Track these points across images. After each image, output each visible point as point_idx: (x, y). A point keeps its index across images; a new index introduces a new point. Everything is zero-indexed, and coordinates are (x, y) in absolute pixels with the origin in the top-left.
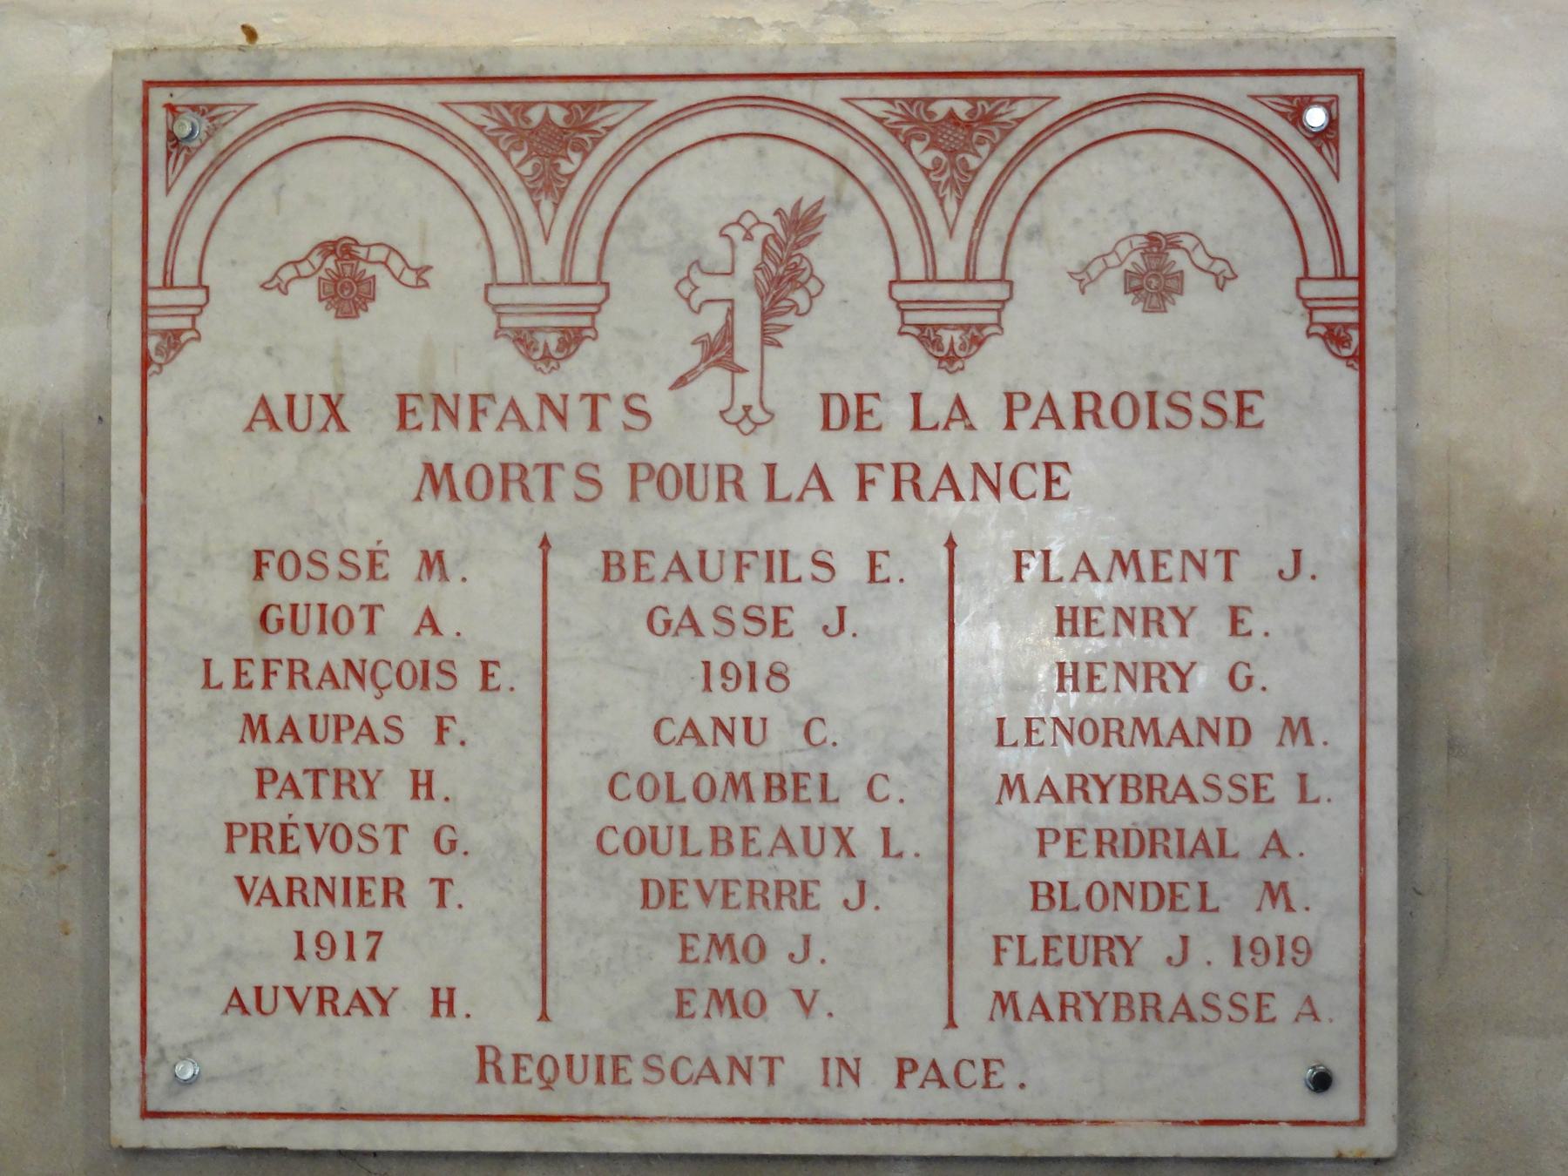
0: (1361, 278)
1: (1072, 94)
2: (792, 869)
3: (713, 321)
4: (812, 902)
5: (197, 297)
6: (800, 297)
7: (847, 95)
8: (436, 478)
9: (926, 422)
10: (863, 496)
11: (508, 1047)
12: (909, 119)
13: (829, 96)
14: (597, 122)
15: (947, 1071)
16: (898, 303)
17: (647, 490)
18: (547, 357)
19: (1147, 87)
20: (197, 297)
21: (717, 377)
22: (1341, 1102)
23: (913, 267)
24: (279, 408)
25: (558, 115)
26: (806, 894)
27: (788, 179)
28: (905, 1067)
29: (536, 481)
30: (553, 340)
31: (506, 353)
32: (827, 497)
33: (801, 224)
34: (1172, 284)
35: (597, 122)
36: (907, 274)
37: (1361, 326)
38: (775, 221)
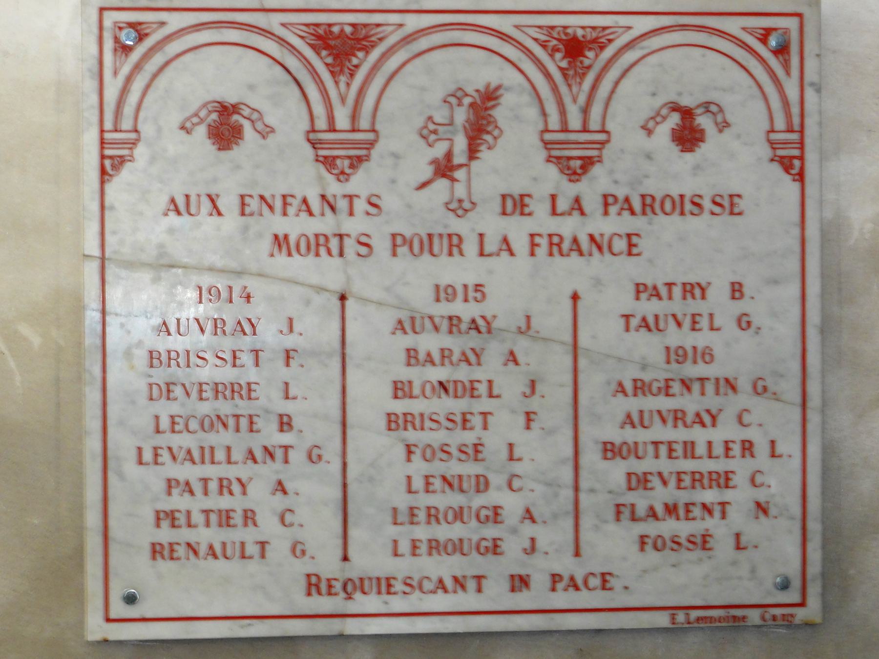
0: (802, 132)
1: (176, 21)
2: (719, 466)
3: (440, 150)
4: (731, 484)
5: (370, 136)
6: (488, 137)
7: (517, 24)
8: (280, 242)
9: (559, 210)
10: (532, 254)
11: (325, 575)
12: (366, 38)
13: (732, 26)
14: (373, 35)
15: (580, 582)
16: (772, 143)
17: (403, 250)
18: (575, 173)
19: (459, 23)
20: (370, 136)
21: (442, 184)
22: (118, 609)
23: (554, 122)
24: (181, 202)
25: (348, 30)
26: (728, 479)
27: (479, 71)
28: (556, 578)
29: (334, 243)
30: (347, 162)
31: (553, 171)
32: (512, 254)
33: (490, 96)
34: (698, 135)
35: (373, 35)
36: (551, 127)
37: (801, 158)
38: (475, 95)
